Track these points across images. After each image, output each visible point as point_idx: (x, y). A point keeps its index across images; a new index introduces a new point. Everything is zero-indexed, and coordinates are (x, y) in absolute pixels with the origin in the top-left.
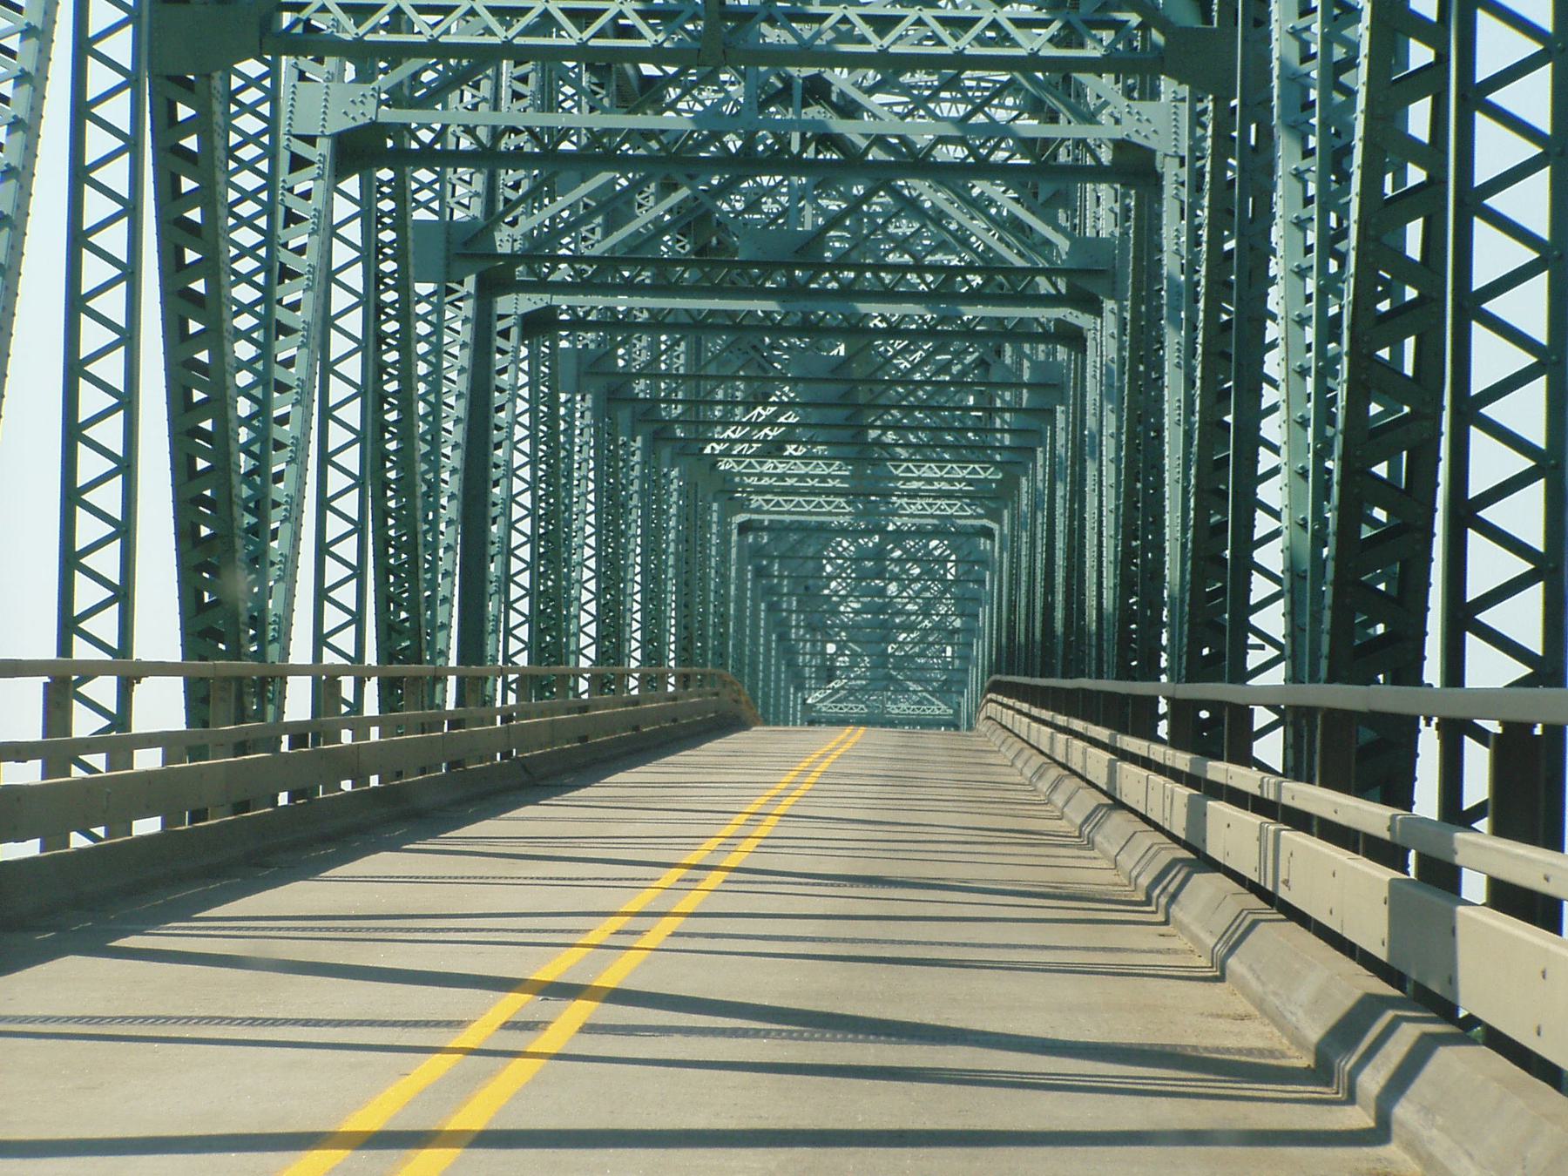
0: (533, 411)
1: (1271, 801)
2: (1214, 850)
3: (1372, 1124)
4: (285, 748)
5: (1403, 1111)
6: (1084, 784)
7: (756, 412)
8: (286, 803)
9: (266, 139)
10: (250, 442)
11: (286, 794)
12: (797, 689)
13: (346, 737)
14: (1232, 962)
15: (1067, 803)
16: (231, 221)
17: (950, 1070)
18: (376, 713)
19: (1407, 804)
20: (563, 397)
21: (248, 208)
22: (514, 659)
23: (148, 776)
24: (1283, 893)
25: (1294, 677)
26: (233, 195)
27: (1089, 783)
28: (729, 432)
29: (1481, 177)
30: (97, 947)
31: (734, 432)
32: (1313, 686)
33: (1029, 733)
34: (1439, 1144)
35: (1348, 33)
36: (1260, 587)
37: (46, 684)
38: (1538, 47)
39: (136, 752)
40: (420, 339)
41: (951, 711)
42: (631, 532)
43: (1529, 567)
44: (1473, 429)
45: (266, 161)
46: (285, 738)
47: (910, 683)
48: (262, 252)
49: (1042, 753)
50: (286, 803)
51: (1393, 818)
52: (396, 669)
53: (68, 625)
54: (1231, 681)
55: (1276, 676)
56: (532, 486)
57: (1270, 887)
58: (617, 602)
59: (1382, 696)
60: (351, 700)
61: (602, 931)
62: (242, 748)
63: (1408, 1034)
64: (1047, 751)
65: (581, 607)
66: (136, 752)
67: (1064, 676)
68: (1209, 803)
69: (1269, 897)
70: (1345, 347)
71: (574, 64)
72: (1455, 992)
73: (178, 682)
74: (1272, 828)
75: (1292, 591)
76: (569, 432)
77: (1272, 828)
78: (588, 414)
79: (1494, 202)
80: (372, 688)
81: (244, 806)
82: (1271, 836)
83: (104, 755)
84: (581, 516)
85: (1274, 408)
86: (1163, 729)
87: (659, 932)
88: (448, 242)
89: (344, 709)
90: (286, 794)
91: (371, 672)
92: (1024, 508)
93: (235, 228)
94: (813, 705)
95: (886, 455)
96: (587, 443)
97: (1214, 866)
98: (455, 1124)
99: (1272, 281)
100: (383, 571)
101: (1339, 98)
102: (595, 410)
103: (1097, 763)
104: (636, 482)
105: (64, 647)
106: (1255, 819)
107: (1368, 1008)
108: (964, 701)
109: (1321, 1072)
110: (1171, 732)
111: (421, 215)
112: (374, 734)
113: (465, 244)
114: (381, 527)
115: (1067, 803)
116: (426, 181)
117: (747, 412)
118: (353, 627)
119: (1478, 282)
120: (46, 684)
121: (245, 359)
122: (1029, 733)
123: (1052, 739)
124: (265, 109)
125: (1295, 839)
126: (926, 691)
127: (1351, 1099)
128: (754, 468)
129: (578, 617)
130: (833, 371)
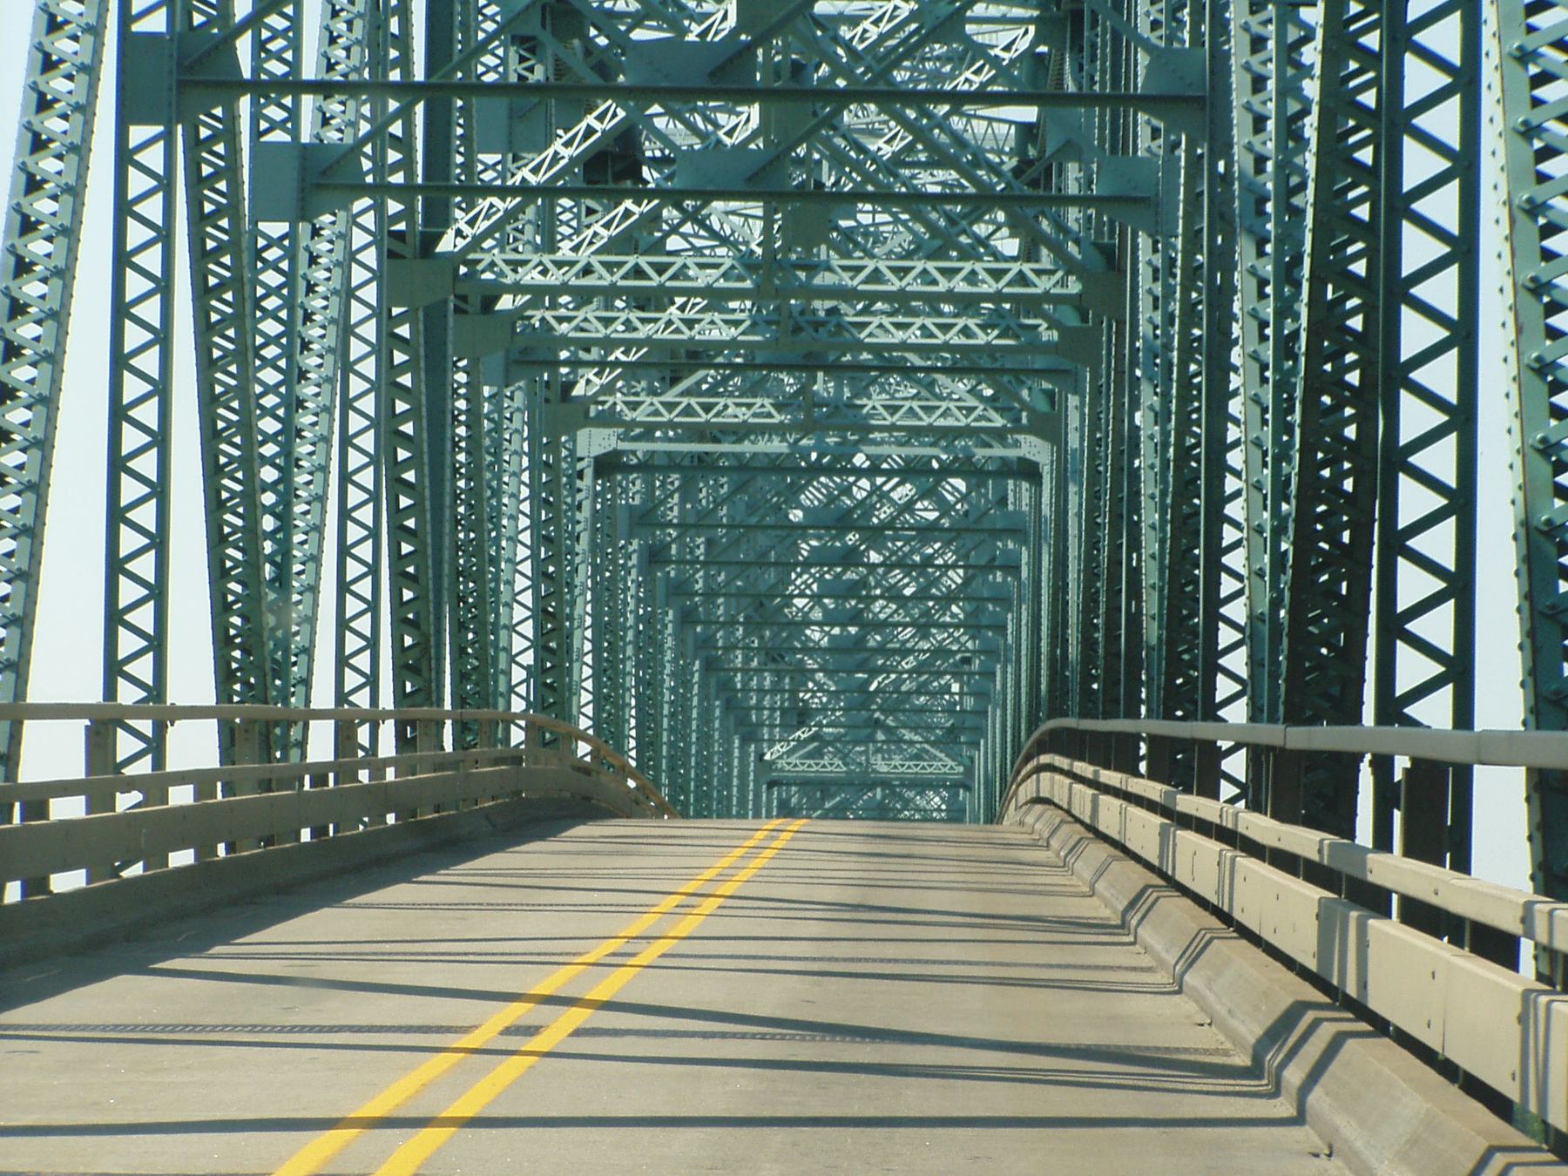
1: (1229, 830)
3: (1295, 1114)
4: (307, 787)
5: (1318, 1098)
6: (1118, 853)
8: (308, 840)
11: (308, 830)
12: (745, 742)
13: (364, 776)
14: (1187, 978)
17: (924, 1066)
18: (393, 754)
19: (1352, 836)
20: (487, 391)
22: (351, 698)
23: (182, 811)
24: (1237, 915)
25: (1254, 716)
30: (142, 969)
31: (535, 171)
32: (1272, 726)
33: (1052, 788)
34: (1349, 1129)
36: (1226, 636)
37: (87, 727)
39: (170, 789)
40: (265, 487)
41: (961, 769)
46: (307, 778)
47: (903, 731)
50: (308, 840)
51: (1321, 841)
52: (469, 712)
53: (114, 668)
57: (1226, 909)
59: (1324, 737)
60: (367, 745)
61: (600, 951)
62: (267, 786)
63: (1326, 1031)
64: (1152, 856)
66: (170, 789)
67: (1084, 714)
68: (1371, 922)
69: (1226, 918)
72: (1366, 996)
73: (213, 724)
74: (1229, 854)
75: (1251, 637)
77: (1229, 854)
80: (387, 730)
81: (269, 841)
82: (1228, 862)
83: (192, 786)
86: (1143, 767)
87: (650, 953)
89: (361, 754)
90: (18, 884)
91: (386, 715)
94: (773, 762)
95: (866, 655)
98: (591, 995)
103: (1143, 830)
105: (110, 691)
106: (1214, 846)
107: (1299, 1008)
108: (979, 757)
109: (1254, 1071)
110: (1149, 767)
112: (390, 774)
113: (521, 352)
118: (150, 655)
120: (87, 727)
122: (1052, 788)
123: (1095, 802)
125: (1249, 865)
126: (927, 741)
127: (1275, 1094)
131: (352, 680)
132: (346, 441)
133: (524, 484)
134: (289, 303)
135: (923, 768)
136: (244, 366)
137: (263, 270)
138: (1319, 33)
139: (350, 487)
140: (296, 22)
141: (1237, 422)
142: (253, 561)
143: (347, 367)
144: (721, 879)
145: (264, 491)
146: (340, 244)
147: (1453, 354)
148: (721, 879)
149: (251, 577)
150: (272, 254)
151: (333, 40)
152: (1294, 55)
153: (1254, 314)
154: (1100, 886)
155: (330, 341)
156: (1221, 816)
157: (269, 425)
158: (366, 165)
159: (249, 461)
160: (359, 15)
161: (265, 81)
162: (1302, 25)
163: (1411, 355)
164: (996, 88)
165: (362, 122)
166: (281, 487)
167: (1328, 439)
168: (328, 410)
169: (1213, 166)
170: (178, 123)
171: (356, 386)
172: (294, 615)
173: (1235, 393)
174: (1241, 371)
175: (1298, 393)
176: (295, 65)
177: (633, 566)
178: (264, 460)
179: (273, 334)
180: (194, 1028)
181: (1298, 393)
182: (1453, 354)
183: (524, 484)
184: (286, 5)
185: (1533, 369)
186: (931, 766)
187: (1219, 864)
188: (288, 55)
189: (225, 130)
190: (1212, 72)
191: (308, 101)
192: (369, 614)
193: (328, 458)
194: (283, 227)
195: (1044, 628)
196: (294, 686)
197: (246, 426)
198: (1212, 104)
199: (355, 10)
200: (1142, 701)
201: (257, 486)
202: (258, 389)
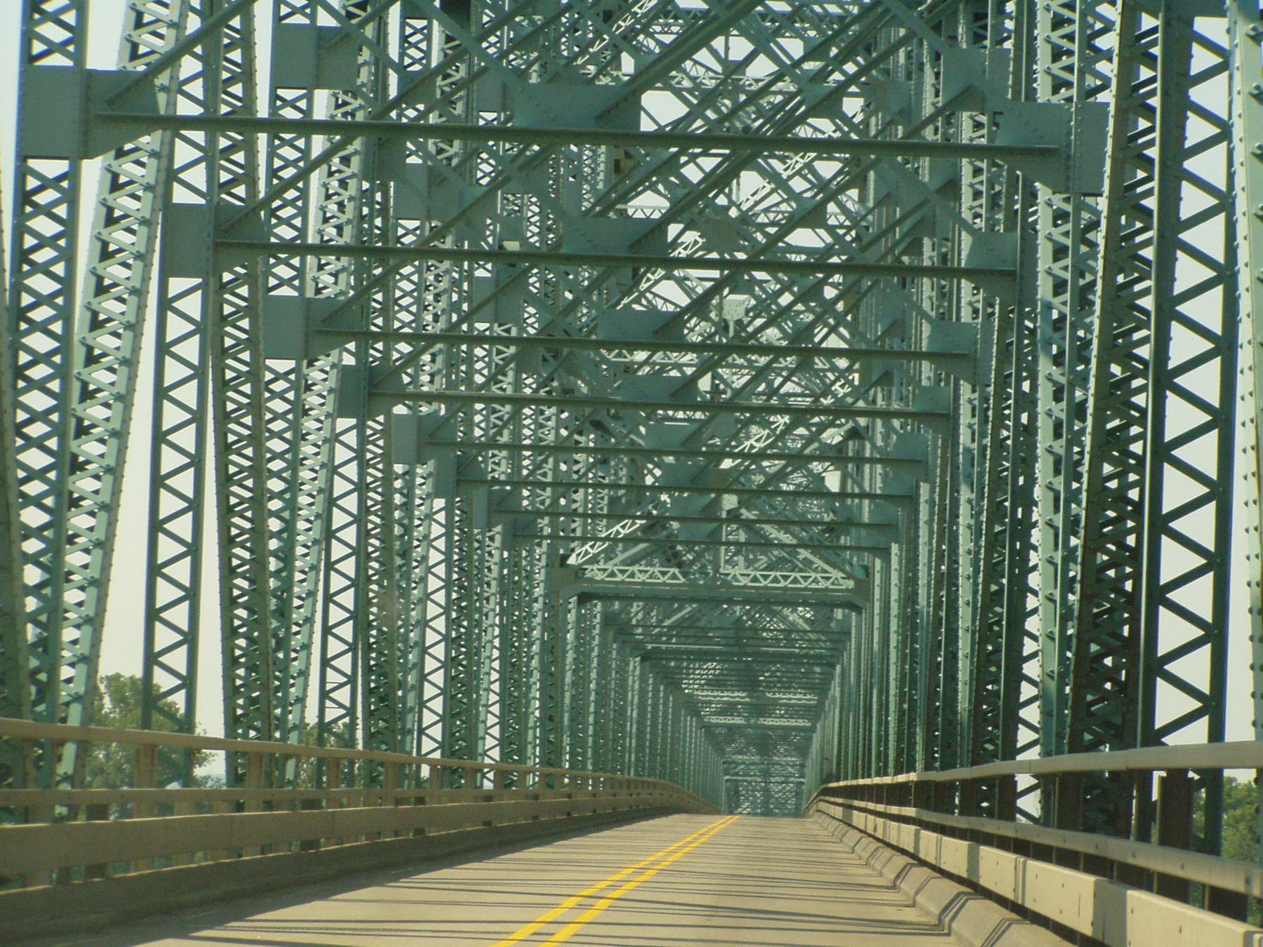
2: (985, 881)
7: (614, 529)
9: (57, 359)
10: (38, 612)
16: (19, 442)
21: (37, 430)
25: (1046, 753)
26: (21, 416)
28: (587, 547)
29: (1167, 508)
35: (1088, 320)
38: (1213, 274)
40: (273, 496)
43: (1212, 346)
44: (1161, 608)
45: (60, 323)
48: (55, 417)
54: (1004, 759)
55: (1033, 754)
56: (448, 585)
70: (1085, 487)
79: (1175, 525)
85: (1035, 611)
93: (22, 449)
97: (987, 894)
99: (1034, 525)
101: (1084, 249)
117: (608, 527)
119: (1164, 579)
124: (57, 327)
130: (683, 444)
132: (329, 598)
135: (795, 581)
136: (258, 417)
138: (1118, 27)
141: (1035, 593)
142: (258, 562)
146: (318, 525)
147: (1214, 434)
149: (257, 572)
150: (279, 386)
151: (328, 197)
152: (1084, 353)
153: (1050, 524)
154: (918, 898)
157: (274, 525)
159: (258, 471)
161: (274, 244)
162: (1098, 75)
163: (1185, 313)
166: (285, 535)
167: (1116, 453)
168: (314, 568)
169: (1015, 481)
171: (338, 550)
173: (1035, 568)
175: (1088, 449)
176: (302, 231)
178: (272, 474)
179: (280, 411)
181: (1088, 449)
182: (1214, 434)
186: (805, 578)
190: (1022, 251)
193: (314, 612)
197: (256, 407)
198: (1022, 278)
200: (956, 807)
202: (268, 376)
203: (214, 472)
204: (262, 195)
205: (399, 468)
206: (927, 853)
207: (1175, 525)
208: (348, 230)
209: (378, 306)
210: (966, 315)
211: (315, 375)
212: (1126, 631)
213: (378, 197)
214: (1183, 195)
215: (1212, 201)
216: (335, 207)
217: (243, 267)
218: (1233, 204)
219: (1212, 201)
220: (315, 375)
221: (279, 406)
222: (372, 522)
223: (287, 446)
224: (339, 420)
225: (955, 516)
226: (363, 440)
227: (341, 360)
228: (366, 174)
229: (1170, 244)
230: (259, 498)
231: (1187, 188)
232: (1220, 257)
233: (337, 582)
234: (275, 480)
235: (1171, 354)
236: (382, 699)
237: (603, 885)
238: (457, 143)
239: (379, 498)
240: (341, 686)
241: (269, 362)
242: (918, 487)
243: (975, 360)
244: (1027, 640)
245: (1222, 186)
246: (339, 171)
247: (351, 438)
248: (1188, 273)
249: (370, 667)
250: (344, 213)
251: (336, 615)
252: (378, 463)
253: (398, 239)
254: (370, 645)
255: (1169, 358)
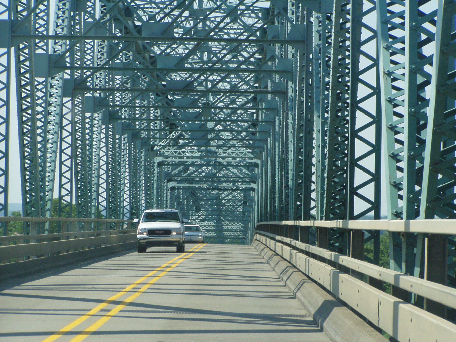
0: (107, 146)
15: (264, 255)
20: (117, 137)
27: (284, 259)
29: (356, 185)
40: (38, 128)
42: (141, 179)
49: (272, 250)
56: (107, 181)
58: (136, 202)
62: (39, 240)
65: (124, 192)
71: (139, 101)
76: (120, 147)
77: (308, 259)
78: (126, 139)
82: (308, 261)
84: (125, 162)
88: (49, 63)
92: (264, 159)
96: (126, 149)
100: (77, 180)
102: (129, 142)
104: (143, 162)
111: (39, 51)
114: (76, 169)
115: (264, 255)
116: (118, 83)
121: (39, 126)
123: (275, 245)
128: (181, 154)
129: (123, 195)
131: (64, 192)
132: (61, 151)
133: (127, 165)
134: (45, 101)
137: (38, 19)
139: (63, 154)
140: (48, 7)
141: (314, 183)
143: (61, 128)
144: (168, 267)
145: (38, 129)
148: (168, 267)
150: (40, 87)
155: (57, 121)
156: (305, 248)
157: (39, 139)
158: (68, 60)
159: (33, 120)
160: (66, 26)
164: (252, 38)
165: (143, 194)
170: (12, 46)
171: (65, 134)
172: (47, 189)
173: (314, 173)
174: (316, 183)
177: (143, 165)
179: (40, 96)
180: (19, 310)
183: (127, 165)
184: (45, 1)
185: (394, 214)
186: (236, 224)
187: (305, 262)
188: (45, 18)
189: (27, 7)
191: (50, 41)
192: (71, 125)
194: (43, 79)
195: (259, 206)
196: (48, 192)
197: (32, 95)
199: (64, 24)
201: (36, 128)
202: (36, 83)
203: (15, 68)
204: (33, 6)
205: (88, 115)
206: (279, 251)
207: (360, 163)
208: (65, 29)
209: (78, 31)
210: (290, 56)
211: (55, 82)
212: (345, 168)
213: (77, 18)
214: (362, 32)
215: (371, 62)
216: (61, 21)
217: (27, 42)
218: (379, 63)
219: (371, 62)
220: (55, 82)
221: (40, 94)
222: (78, 135)
223: (43, 109)
224: (64, 98)
225: (287, 128)
226: (74, 105)
227: (63, 76)
228: (71, 9)
229: (356, 80)
230: (34, 128)
231: (362, 58)
232: (375, 85)
233: (65, 145)
234: (39, 107)
235: (358, 96)
236: (83, 191)
237: (165, 265)
238: (106, 41)
239: (80, 126)
240: (67, 195)
241: (36, 78)
242: (275, 118)
243: (293, 73)
244: (312, 201)
245: (375, 57)
246: (62, 17)
247: (69, 105)
248: (362, 91)
249: (78, 180)
250: (64, 23)
251: (64, 157)
252: (80, 113)
253: (85, 63)
254: (78, 164)
255: (357, 97)
